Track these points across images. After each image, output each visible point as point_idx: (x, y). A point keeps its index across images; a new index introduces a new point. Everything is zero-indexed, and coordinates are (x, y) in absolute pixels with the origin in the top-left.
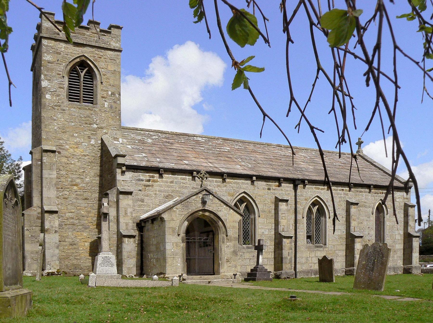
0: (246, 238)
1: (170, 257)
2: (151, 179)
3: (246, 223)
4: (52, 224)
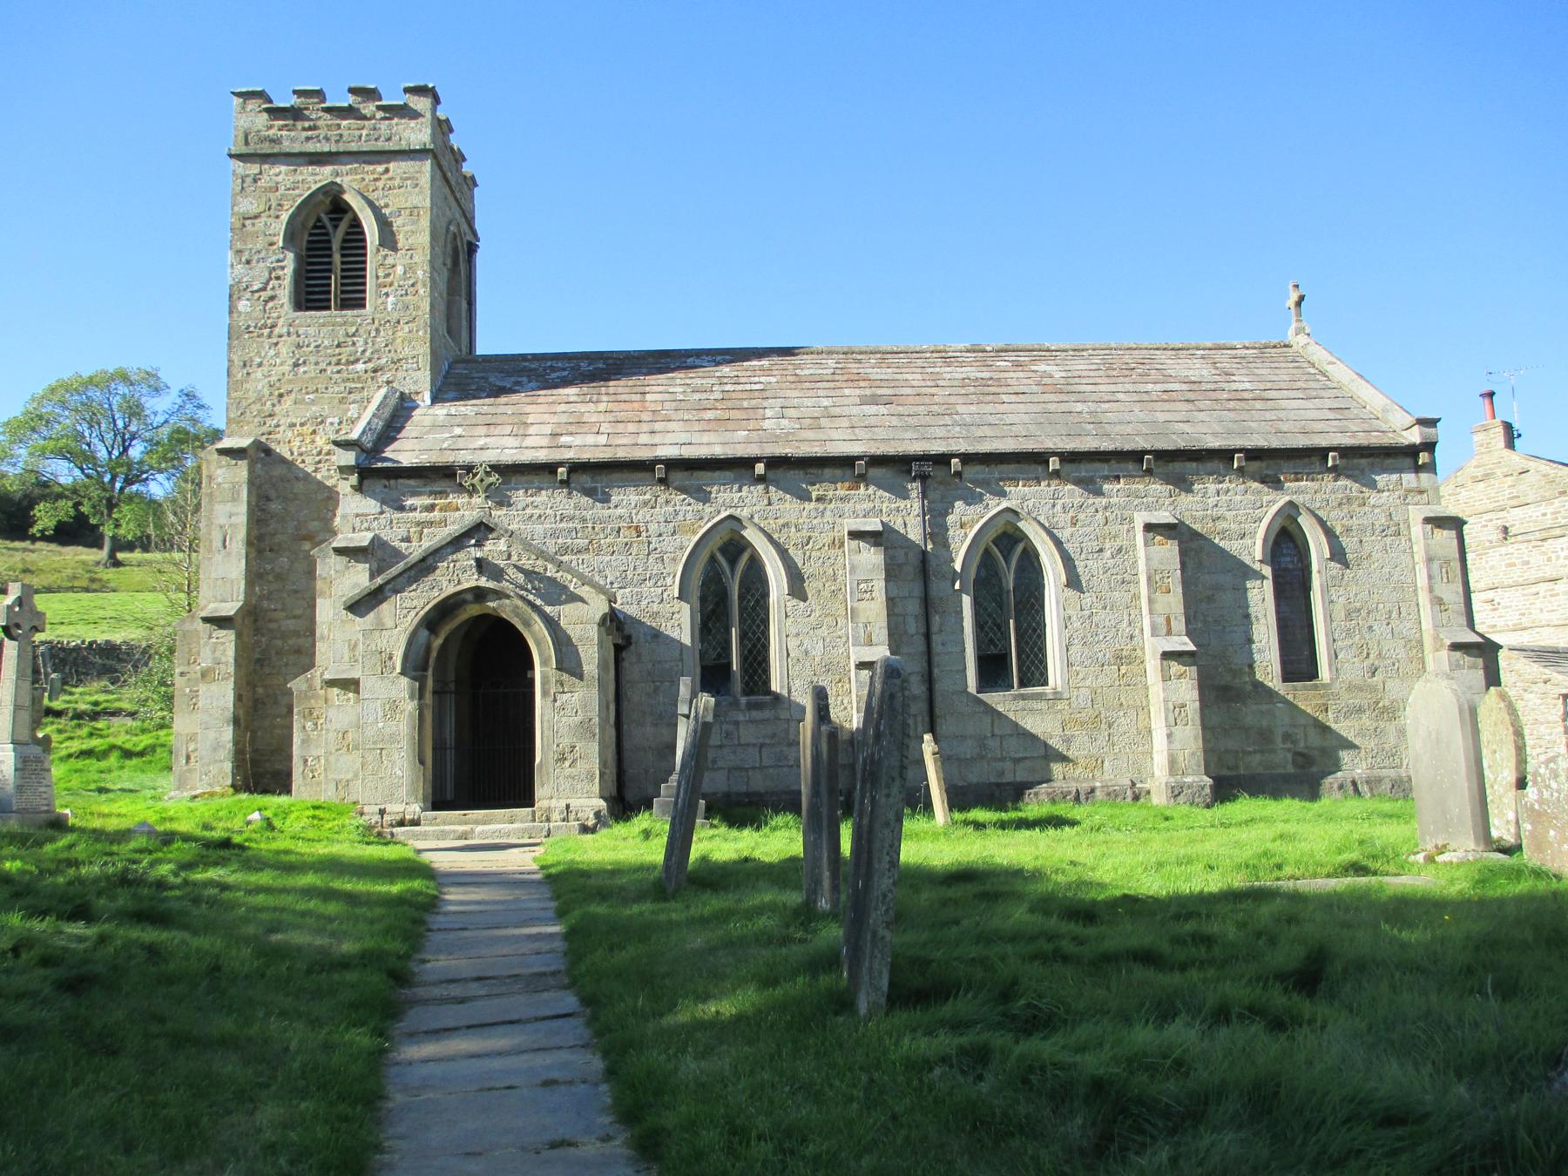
0: (755, 671)
1: (373, 746)
2: (436, 502)
3: (754, 621)
4: (218, 654)
